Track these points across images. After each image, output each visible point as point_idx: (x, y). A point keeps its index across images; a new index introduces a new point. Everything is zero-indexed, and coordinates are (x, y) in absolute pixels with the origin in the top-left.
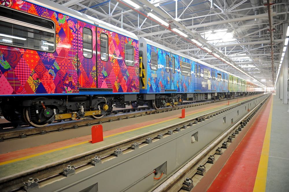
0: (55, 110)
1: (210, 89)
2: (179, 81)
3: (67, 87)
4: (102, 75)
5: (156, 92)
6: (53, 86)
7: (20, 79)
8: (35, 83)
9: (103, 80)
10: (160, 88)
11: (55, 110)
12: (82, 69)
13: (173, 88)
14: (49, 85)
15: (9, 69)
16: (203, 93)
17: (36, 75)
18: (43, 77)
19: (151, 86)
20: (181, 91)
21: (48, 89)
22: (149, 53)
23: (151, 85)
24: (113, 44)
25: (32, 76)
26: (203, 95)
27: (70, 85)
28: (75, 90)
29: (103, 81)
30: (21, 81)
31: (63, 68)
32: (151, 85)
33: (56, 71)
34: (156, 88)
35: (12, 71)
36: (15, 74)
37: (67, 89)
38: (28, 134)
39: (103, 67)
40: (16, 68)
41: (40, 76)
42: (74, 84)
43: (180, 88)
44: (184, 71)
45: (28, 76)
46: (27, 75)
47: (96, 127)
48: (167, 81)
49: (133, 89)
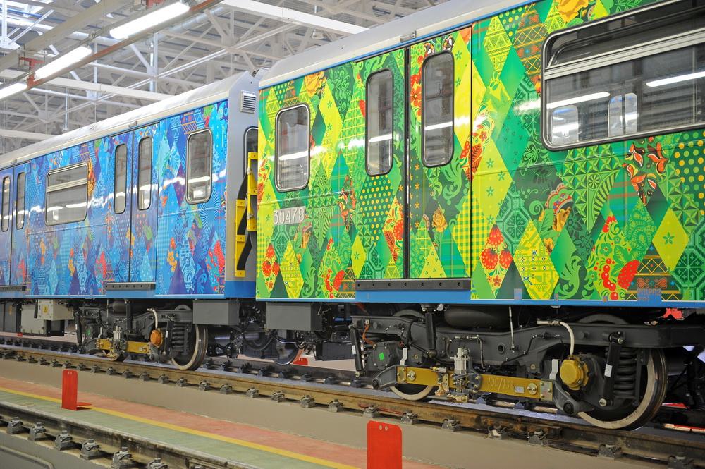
13: (146, 277)
20: (83, 289)
22: (174, 147)
23: (76, 268)
32: (76, 268)
34: (198, 275)
43: (83, 276)
44: (72, 202)
47: (381, 427)
48: (39, 257)
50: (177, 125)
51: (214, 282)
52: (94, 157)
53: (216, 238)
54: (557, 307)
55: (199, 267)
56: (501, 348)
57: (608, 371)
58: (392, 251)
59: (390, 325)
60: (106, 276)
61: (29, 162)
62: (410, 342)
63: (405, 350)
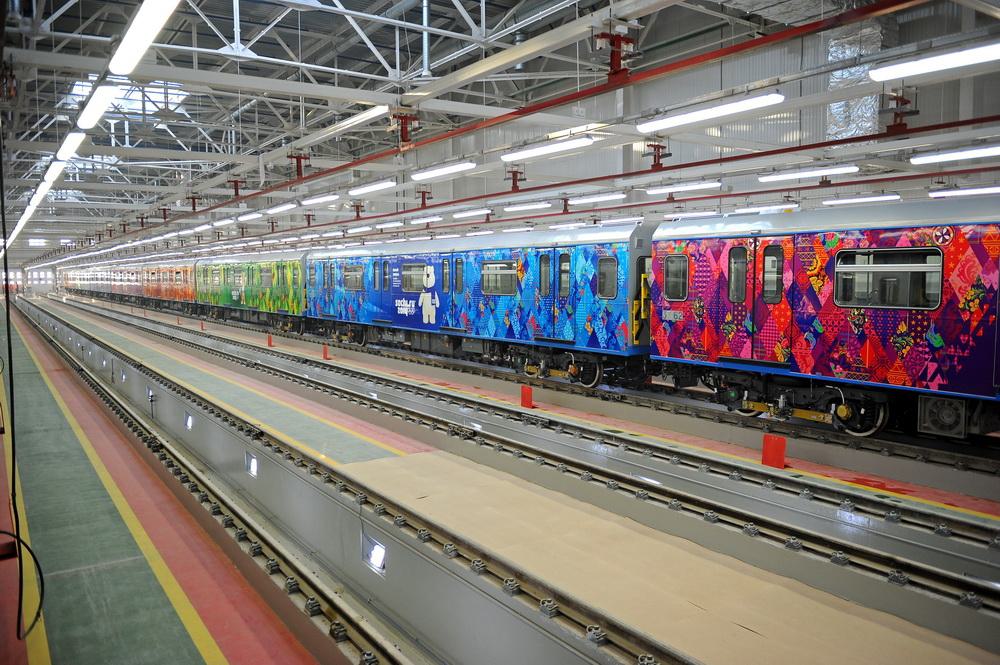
1: (433, 321)
2: (511, 311)
6: (811, 361)
10: (530, 332)
12: (870, 332)
14: (803, 358)
15: (941, 347)
19: (511, 326)
22: (589, 261)
24: (976, 259)
29: (745, 343)
31: (830, 329)
33: (816, 334)
37: (835, 368)
38: (973, 466)
39: (929, 325)
41: (791, 344)
42: (849, 358)
49: (685, 352)
50: (592, 250)
53: (622, 320)
54: (299, 10)
56: (804, 397)
58: (307, 80)
60: (535, 330)
62: (529, 356)
63: (746, 392)
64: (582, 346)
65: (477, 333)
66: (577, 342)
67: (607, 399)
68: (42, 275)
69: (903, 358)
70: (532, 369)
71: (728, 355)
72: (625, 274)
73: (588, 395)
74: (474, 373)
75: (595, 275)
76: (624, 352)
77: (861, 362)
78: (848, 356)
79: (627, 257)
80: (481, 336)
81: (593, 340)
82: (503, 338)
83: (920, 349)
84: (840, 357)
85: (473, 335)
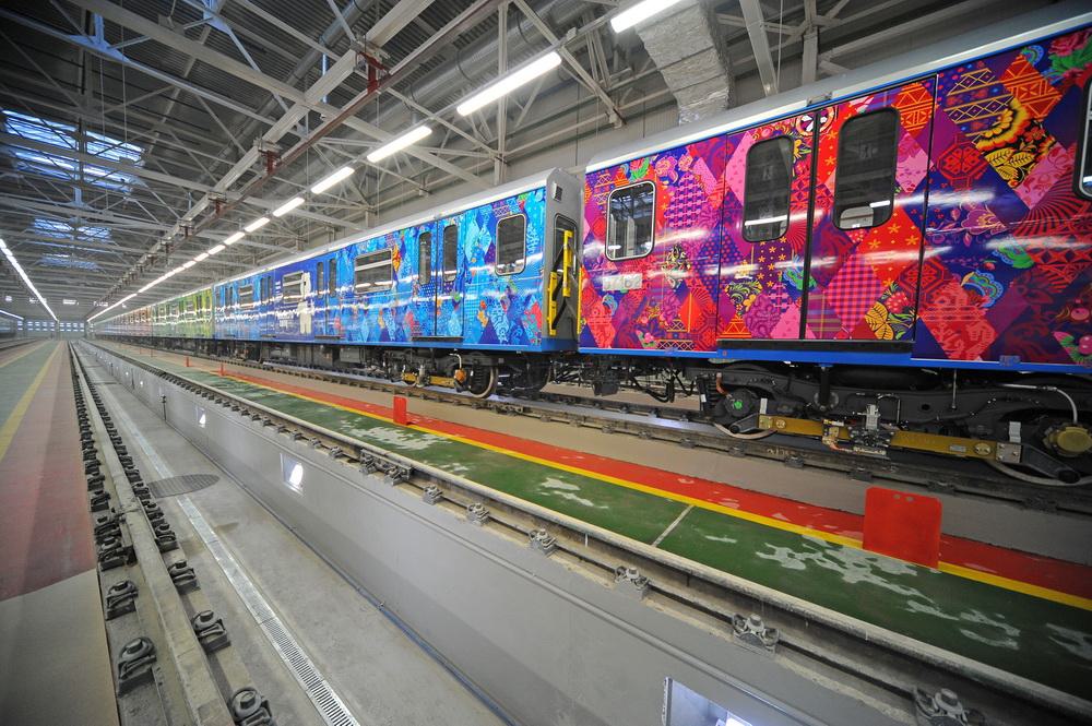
0: (764, 402)
3: (645, 333)
4: (783, 286)
5: (510, 342)
6: (611, 331)
7: (841, 313)
8: (896, 321)
9: (784, 306)
11: (764, 402)
13: (455, 332)
14: (602, 328)
16: (312, 344)
17: (901, 297)
18: (931, 303)
21: (952, 342)
22: (484, 228)
25: (883, 302)
26: (305, 350)
27: (654, 328)
28: (667, 341)
30: (845, 317)
35: (820, 293)
36: (826, 301)
40: (831, 284)
42: (663, 322)
45: (871, 303)
46: (868, 299)
50: (486, 212)
51: (530, 335)
52: (400, 243)
55: (513, 324)
57: (472, 374)
59: (399, 355)
61: (341, 251)
62: (406, 362)
64: (472, 343)
65: (350, 339)
66: (466, 337)
67: (504, 412)
68: (75, 325)
69: (744, 312)
70: (411, 377)
71: (743, 335)
72: (539, 234)
73: (479, 407)
74: (352, 384)
75: (492, 245)
76: (536, 347)
77: (681, 325)
78: (662, 318)
79: (542, 209)
80: (354, 342)
81: (489, 334)
82: (376, 342)
83: (773, 296)
84: (649, 322)
85: (347, 342)
